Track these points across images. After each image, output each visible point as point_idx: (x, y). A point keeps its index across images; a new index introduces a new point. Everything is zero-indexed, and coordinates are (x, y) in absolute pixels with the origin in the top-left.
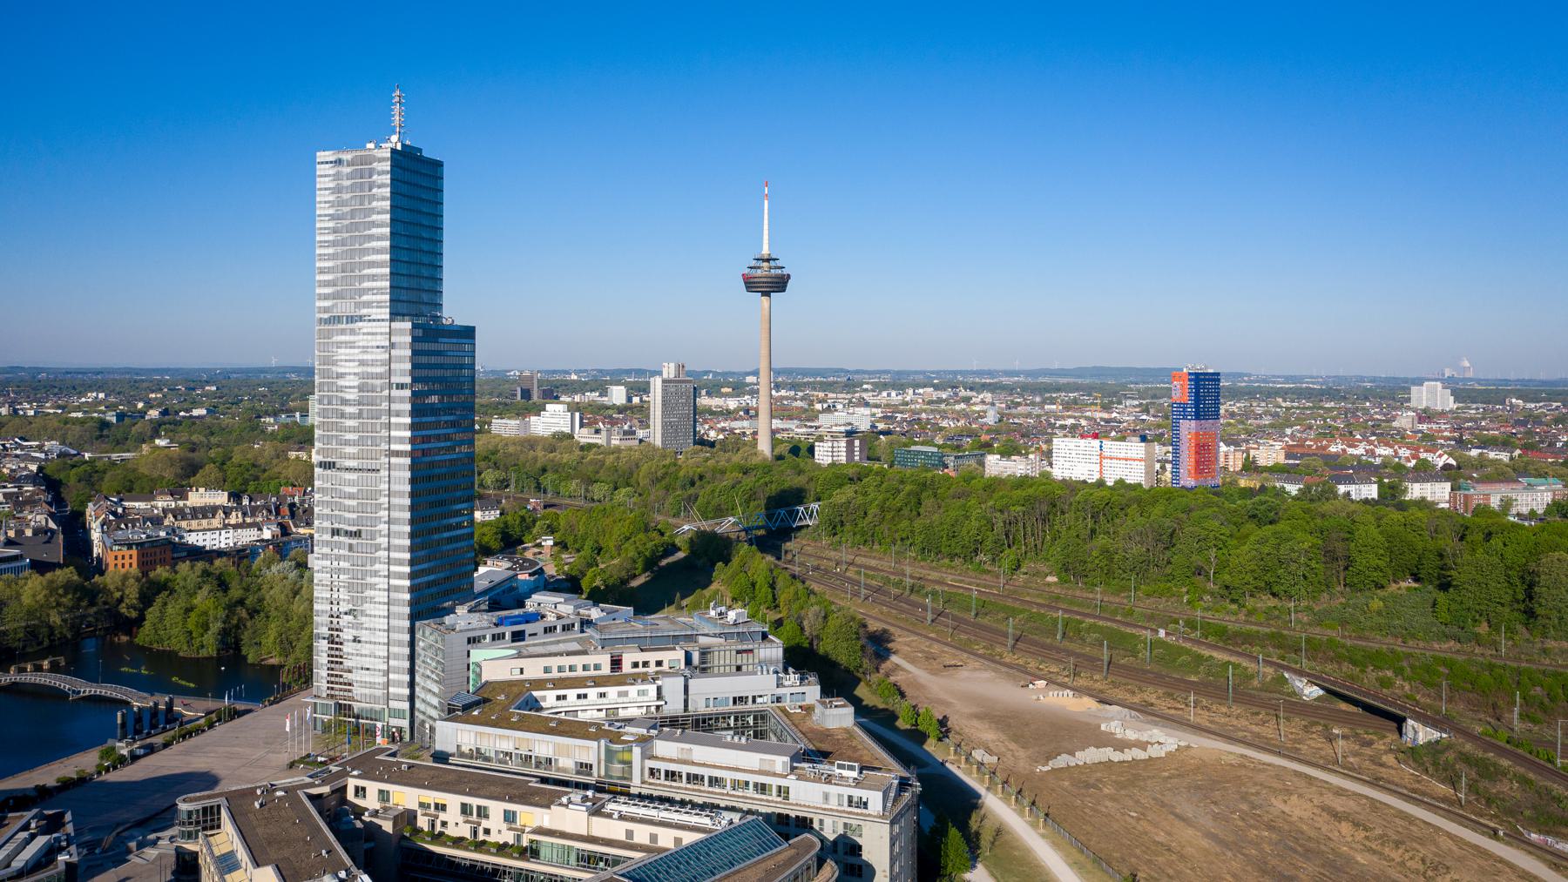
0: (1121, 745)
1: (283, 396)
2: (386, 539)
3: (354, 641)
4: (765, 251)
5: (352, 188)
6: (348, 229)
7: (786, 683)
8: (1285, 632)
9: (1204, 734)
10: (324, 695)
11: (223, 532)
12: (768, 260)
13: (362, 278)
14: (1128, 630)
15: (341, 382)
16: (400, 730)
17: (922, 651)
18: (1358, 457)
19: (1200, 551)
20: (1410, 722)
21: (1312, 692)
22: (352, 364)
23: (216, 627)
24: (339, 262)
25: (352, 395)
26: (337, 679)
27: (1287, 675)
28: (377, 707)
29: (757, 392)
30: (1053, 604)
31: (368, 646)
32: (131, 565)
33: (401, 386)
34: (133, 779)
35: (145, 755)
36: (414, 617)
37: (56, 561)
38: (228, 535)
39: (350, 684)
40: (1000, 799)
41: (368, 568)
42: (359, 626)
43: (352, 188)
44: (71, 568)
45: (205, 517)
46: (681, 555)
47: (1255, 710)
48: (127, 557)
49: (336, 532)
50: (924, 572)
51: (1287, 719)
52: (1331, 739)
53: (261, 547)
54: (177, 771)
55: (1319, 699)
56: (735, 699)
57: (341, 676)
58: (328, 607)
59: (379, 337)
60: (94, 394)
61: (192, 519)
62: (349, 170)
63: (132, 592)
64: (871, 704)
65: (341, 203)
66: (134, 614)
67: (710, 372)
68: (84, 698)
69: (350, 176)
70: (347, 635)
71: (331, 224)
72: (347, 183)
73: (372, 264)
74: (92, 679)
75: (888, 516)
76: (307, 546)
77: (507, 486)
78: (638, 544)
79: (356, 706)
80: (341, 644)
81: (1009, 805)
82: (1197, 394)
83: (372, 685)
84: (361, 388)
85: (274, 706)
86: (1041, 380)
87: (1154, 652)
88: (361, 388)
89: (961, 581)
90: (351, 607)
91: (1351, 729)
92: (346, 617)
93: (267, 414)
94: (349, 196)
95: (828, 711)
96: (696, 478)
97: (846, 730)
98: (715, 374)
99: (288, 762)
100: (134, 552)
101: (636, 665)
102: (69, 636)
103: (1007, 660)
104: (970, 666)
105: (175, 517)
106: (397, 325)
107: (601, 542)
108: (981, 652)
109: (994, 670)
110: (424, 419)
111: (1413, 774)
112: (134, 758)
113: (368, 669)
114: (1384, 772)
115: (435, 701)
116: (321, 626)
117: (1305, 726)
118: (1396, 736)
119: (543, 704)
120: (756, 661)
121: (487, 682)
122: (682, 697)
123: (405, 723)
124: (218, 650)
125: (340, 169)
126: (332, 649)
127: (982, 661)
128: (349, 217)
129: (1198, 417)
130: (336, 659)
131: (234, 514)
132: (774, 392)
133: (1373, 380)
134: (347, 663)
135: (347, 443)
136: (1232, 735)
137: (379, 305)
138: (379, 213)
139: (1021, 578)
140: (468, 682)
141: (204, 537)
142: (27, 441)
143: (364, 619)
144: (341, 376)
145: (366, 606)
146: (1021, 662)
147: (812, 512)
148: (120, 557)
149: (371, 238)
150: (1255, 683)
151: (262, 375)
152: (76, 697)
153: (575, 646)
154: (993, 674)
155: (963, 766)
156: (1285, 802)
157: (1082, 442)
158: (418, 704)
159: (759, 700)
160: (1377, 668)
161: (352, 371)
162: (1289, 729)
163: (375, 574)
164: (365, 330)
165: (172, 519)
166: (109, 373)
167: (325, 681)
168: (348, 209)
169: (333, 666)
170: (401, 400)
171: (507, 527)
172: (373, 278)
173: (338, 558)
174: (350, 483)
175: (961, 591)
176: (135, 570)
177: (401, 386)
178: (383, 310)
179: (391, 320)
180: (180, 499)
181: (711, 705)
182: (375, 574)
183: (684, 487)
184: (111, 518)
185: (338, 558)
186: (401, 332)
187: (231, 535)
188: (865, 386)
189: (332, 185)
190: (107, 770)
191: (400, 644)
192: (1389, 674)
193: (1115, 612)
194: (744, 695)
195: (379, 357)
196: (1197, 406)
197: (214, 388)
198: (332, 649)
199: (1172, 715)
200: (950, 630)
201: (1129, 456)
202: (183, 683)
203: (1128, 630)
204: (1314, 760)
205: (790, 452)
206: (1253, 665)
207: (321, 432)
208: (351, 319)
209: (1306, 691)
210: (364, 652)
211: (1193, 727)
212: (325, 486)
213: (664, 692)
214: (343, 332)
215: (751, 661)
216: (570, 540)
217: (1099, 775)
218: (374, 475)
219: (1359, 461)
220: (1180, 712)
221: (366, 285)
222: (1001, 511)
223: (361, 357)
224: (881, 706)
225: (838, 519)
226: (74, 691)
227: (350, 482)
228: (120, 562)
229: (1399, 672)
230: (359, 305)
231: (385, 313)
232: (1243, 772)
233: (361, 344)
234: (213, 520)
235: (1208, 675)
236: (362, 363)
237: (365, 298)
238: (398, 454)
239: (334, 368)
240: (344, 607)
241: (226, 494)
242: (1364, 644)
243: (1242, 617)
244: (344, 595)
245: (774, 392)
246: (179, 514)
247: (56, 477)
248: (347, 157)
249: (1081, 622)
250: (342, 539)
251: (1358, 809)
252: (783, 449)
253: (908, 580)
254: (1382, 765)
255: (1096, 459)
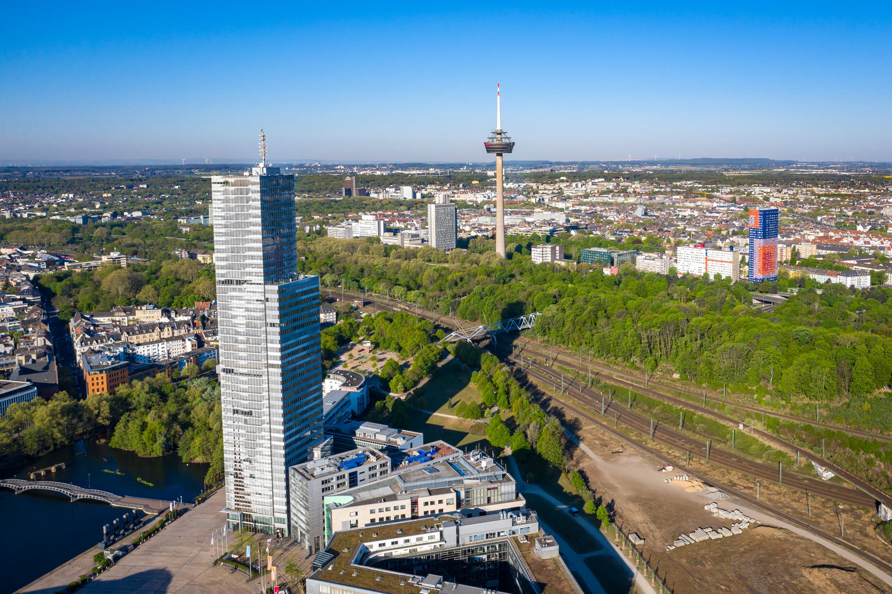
0: (718, 525)
1: (191, 193)
2: (268, 418)
3: (251, 477)
4: (499, 128)
5: (236, 200)
6: (235, 225)
7: (518, 522)
8: (813, 425)
9: (765, 511)
10: (234, 508)
11: (160, 344)
12: (500, 134)
13: (245, 257)
14: (722, 422)
15: (234, 321)
16: (282, 530)
17: (599, 439)
18: (859, 248)
19: (764, 366)
20: (883, 506)
21: (827, 475)
22: (241, 310)
23: (161, 440)
24: (230, 246)
25: (242, 329)
26: (241, 499)
27: (813, 463)
28: (267, 516)
29: (495, 183)
30: (677, 398)
31: (259, 480)
32: (103, 389)
33: (273, 325)
34: (117, 578)
35: (123, 555)
36: (288, 464)
37: (53, 382)
38: (163, 346)
39: (249, 503)
40: (645, 577)
41: (258, 434)
42: (254, 469)
43: (236, 200)
44: (64, 392)
45: (147, 332)
46: (450, 357)
47: (795, 489)
48: (100, 378)
49: (235, 412)
50: (601, 369)
51: (813, 496)
52: (837, 513)
53: (185, 359)
54: (143, 570)
55: (831, 479)
56: (487, 535)
57: (243, 498)
58: (233, 456)
59: (257, 294)
60: (66, 195)
61: (140, 334)
62: (233, 188)
63: (105, 410)
64: (568, 491)
65: (229, 209)
66: (107, 423)
67: (465, 165)
68: (80, 500)
69: (234, 193)
70: (246, 473)
71: (223, 222)
72: (232, 197)
73: (251, 249)
74: (84, 484)
75: (577, 328)
76: (215, 357)
77: (339, 284)
78: (424, 354)
79: (254, 516)
80: (243, 478)
81: (650, 583)
82: (764, 223)
83: (263, 504)
84: (248, 325)
85: (202, 505)
86: (671, 168)
87: (737, 441)
88: (248, 325)
89: (622, 377)
90: (247, 457)
91: (850, 505)
92: (244, 463)
93: (182, 214)
94: (234, 205)
95: (544, 549)
96: (458, 280)
97: (554, 559)
98: (468, 166)
99: (213, 560)
100: (104, 375)
101: (426, 504)
102: (66, 443)
103: (649, 446)
104: (627, 453)
105: (128, 333)
106: (268, 287)
107: (400, 344)
108: (634, 438)
109: (643, 456)
110: (288, 343)
111: (884, 544)
112: (117, 558)
113: (260, 494)
114: (867, 542)
115: (303, 518)
116: (229, 467)
117: (823, 502)
118: (874, 512)
119: (371, 550)
120: (499, 493)
121: (336, 533)
122: (455, 536)
123: (285, 526)
124: (163, 453)
125: (227, 187)
126: (237, 481)
127: (634, 446)
128: (234, 218)
129: (764, 237)
130: (240, 487)
131: (166, 328)
132: (505, 185)
133: (871, 165)
134: (247, 490)
135: (240, 358)
136: (781, 511)
137: (257, 274)
138: (253, 217)
139: (658, 374)
140: (323, 507)
141: (148, 348)
142: (25, 250)
143: (256, 464)
144: (234, 317)
145: (257, 457)
146: (658, 447)
147: (531, 319)
148: (95, 379)
149: (250, 232)
150: (795, 467)
151: (176, 171)
152: (75, 499)
153: (387, 491)
154: (641, 459)
155: (623, 548)
156: (810, 573)
157: (695, 250)
158: (292, 516)
159: (502, 534)
160: (866, 452)
161: (241, 314)
162: (812, 504)
163: (262, 438)
164: (248, 290)
165: (127, 335)
166: (75, 171)
167: (233, 500)
168: (234, 213)
169: (238, 491)
170: (274, 333)
171: (341, 332)
172: (253, 257)
173: (239, 427)
174: (243, 382)
175: (622, 385)
176: (106, 393)
177: (273, 325)
178: (260, 278)
179: (265, 284)
180: (130, 314)
181: (473, 539)
182: (262, 438)
183: (450, 287)
184: (87, 336)
185: (239, 427)
186: (272, 292)
187: (165, 345)
188: (562, 178)
189: (222, 197)
190: (100, 572)
191: (279, 479)
192: (873, 456)
193: (713, 406)
194: (492, 532)
195: (258, 307)
196: (764, 228)
197: (145, 186)
198: (237, 481)
199: (746, 494)
200: (616, 420)
201: (723, 259)
202: (145, 482)
203: (722, 422)
204: (828, 533)
205: (516, 250)
206: (793, 455)
207: (223, 359)
208: (239, 282)
209: (825, 475)
210: (257, 484)
211: (756, 503)
212: (228, 391)
213: (444, 536)
214: (234, 290)
215: (496, 493)
216: (380, 340)
217: (703, 552)
218: (258, 378)
219: (861, 251)
220: (751, 491)
221: (248, 261)
222: (646, 330)
223: (247, 306)
224: (574, 493)
225: (546, 326)
226: (73, 496)
227: (243, 383)
228: (95, 381)
229: (878, 455)
230: (243, 274)
231: (261, 280)
232: (786, 546)
233: (246, 298)
234: (153, 334)
235: (768, 460)
236: (247, 310)
237: (247, 270)
238: (273, 366)
239: (230, 312)
240: (243, 457)
241: (160, 311)
242: (858, 435)
243: (788, 410)
244: (242, 449)
245: (505, 185)
246: (130, 330)
247: (47, 286)
248: (231, 180)
249: (694, 414)
250: (240, 416)
251: (851, 582)
252: (512, 246)
253: (590, 375)
254: (866, 535)
255: (703, 260)
